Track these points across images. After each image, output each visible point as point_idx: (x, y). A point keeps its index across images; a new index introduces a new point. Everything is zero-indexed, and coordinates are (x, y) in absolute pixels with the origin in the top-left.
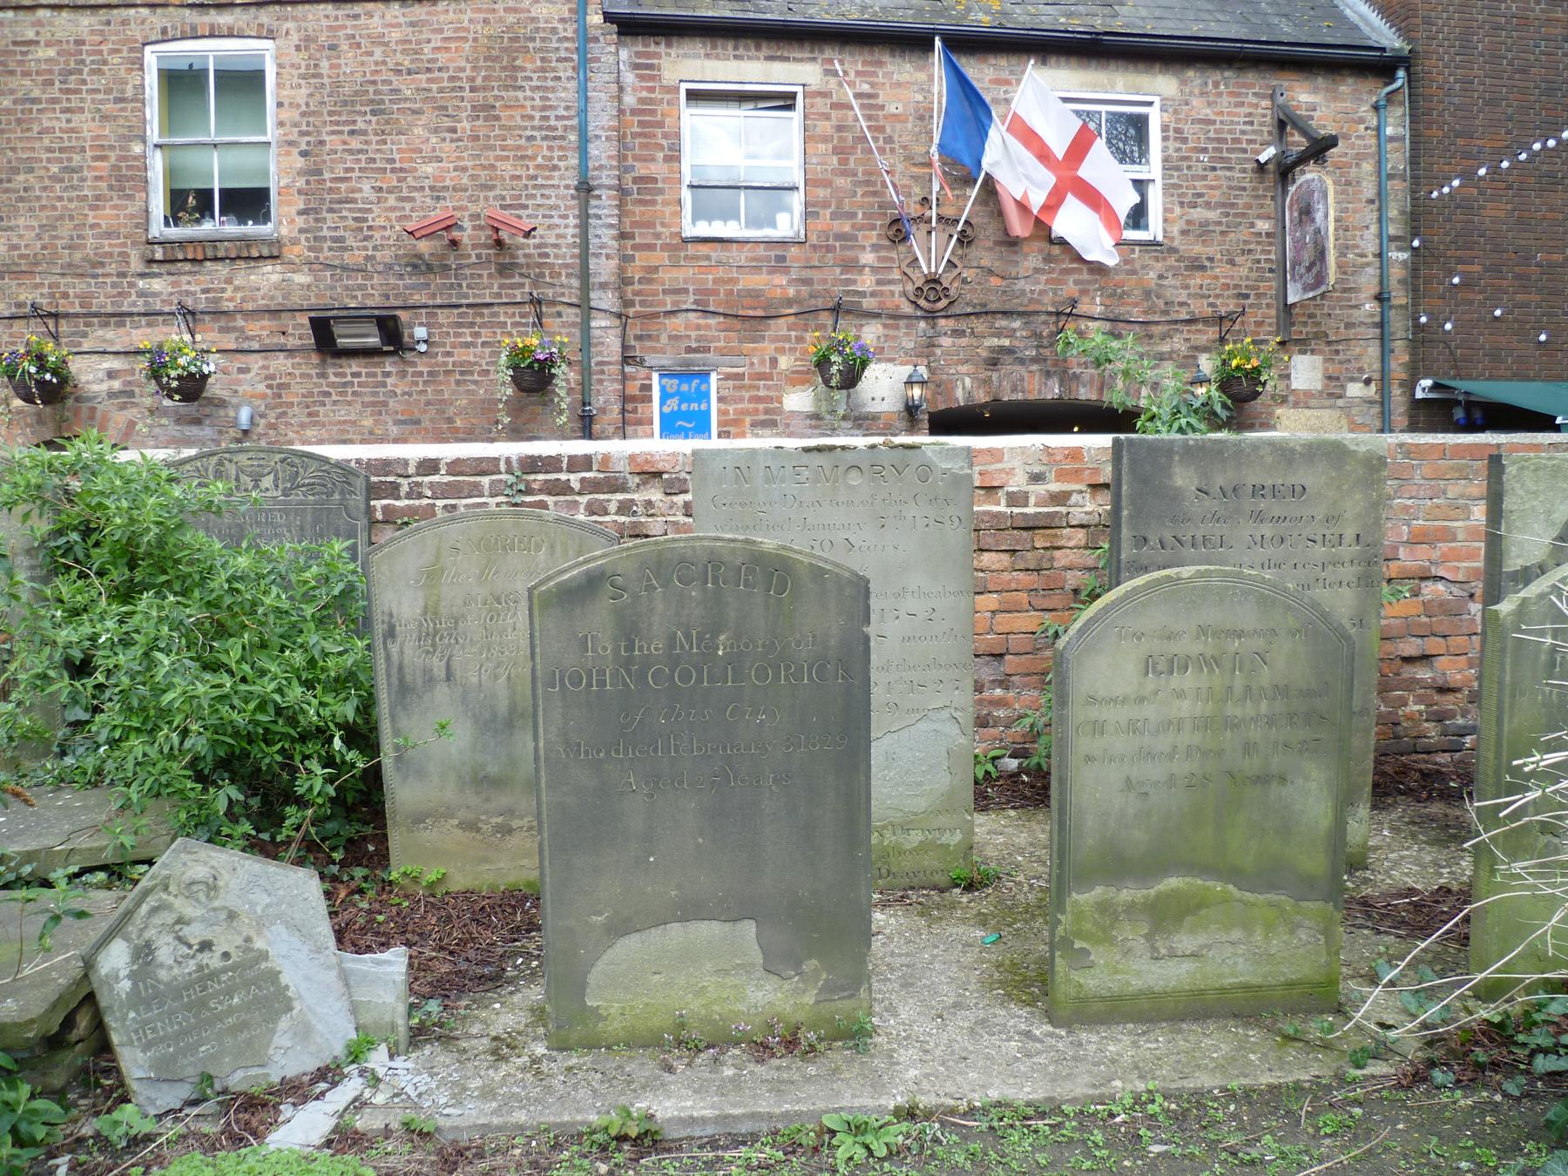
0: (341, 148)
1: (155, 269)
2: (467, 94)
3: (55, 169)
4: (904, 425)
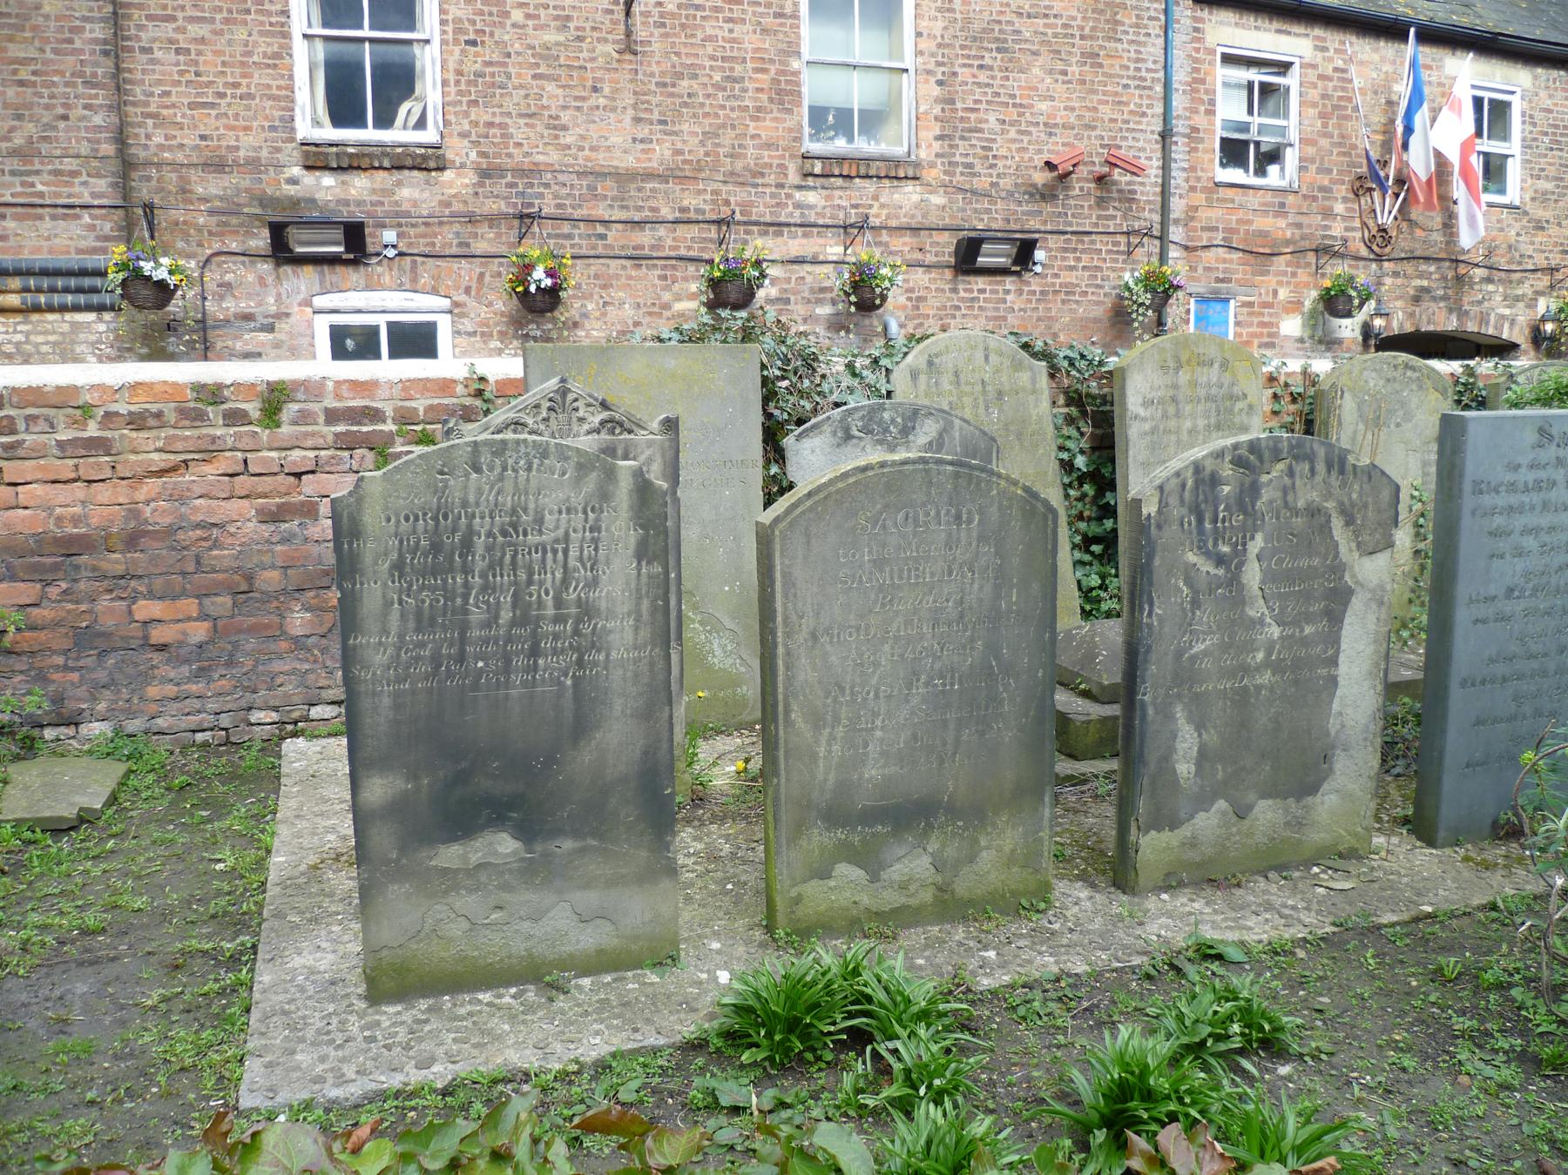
0: (971, 80)
1: (810, 181)
2: (1077, 41)
3: (717, 77)
4: (1360, 348)
